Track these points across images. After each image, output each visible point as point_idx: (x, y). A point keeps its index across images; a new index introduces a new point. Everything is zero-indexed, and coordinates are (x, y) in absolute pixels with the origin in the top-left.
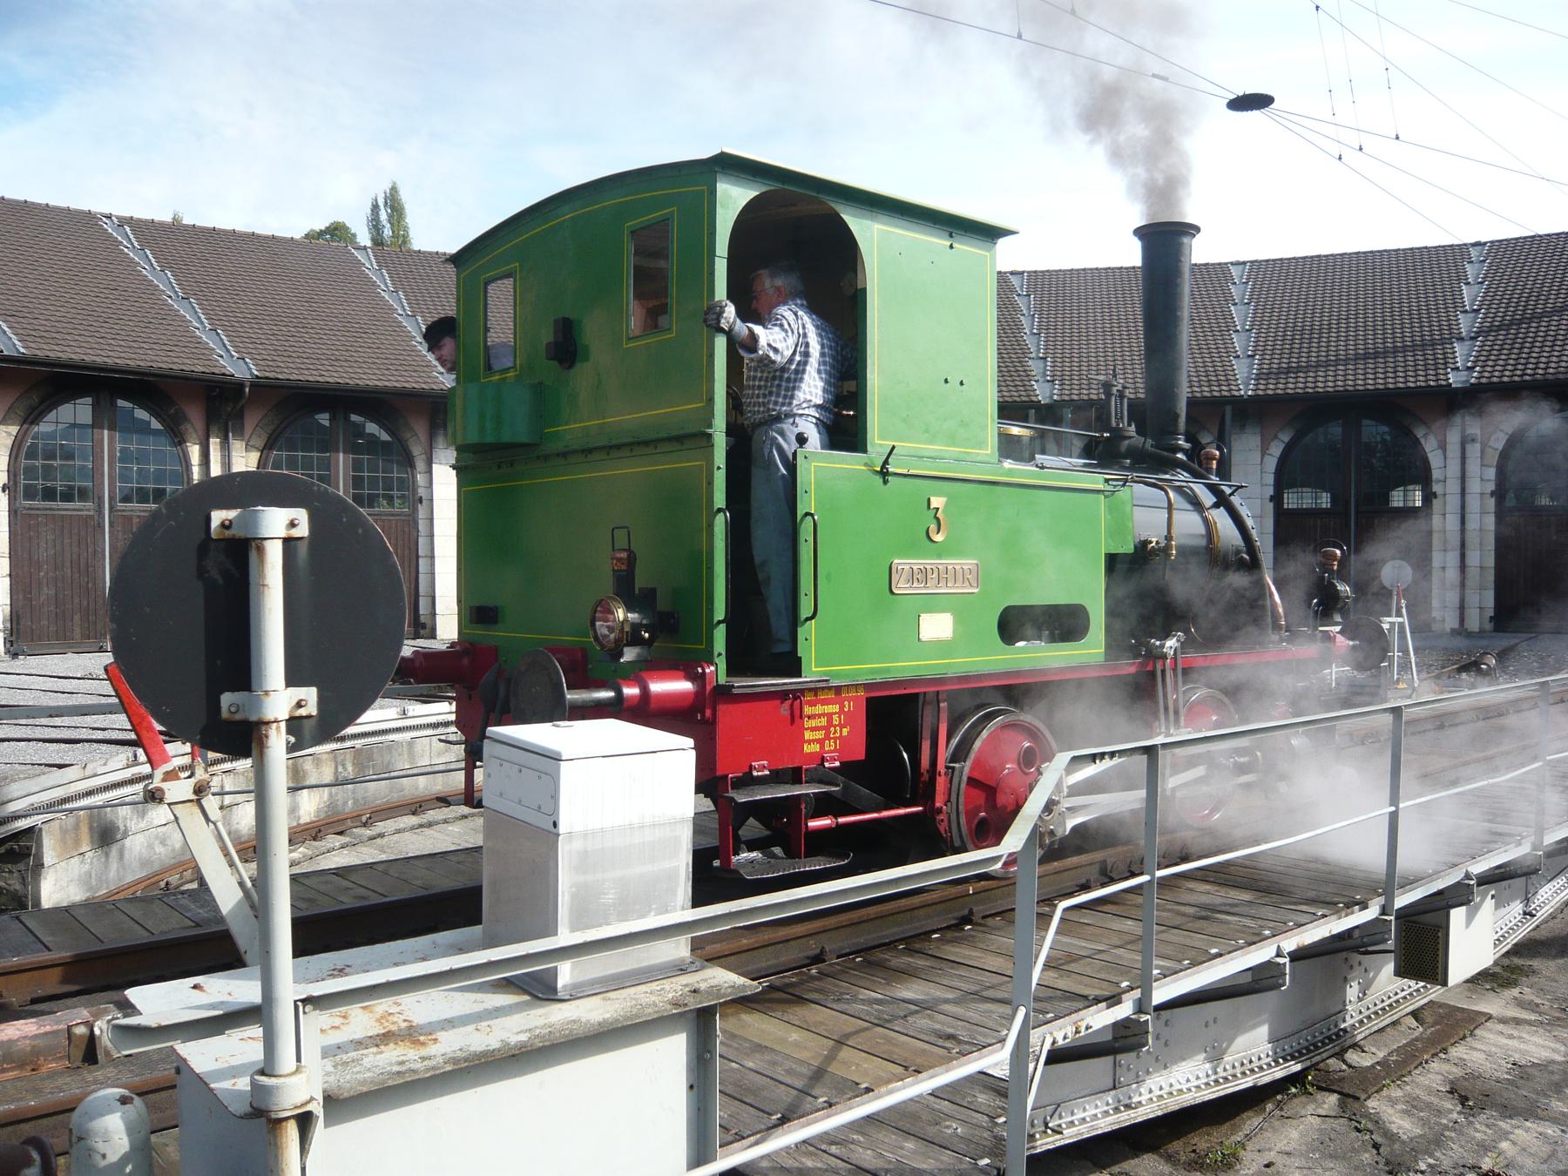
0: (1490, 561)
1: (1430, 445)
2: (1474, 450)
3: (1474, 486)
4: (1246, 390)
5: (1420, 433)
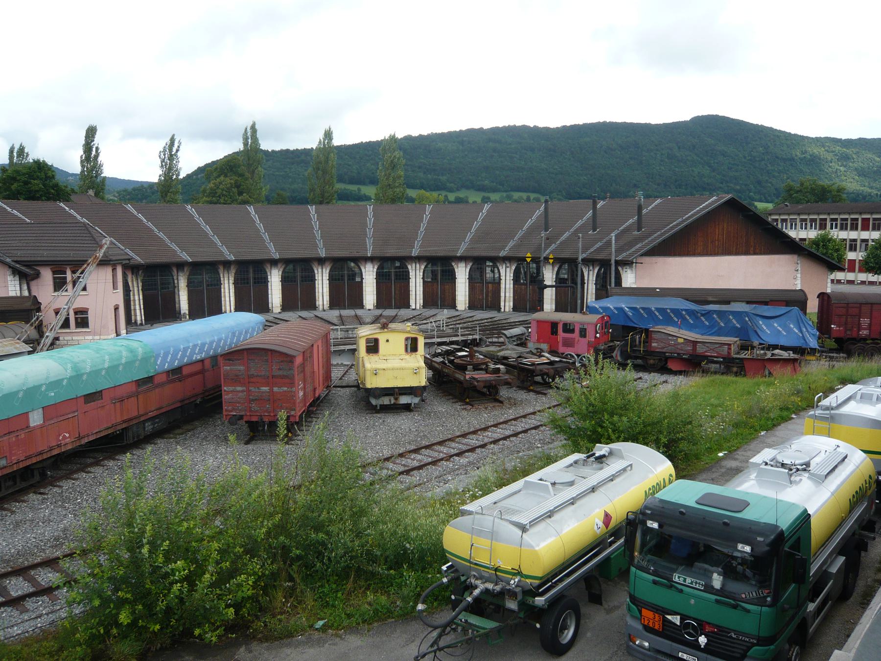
0: (512, 295)
1: (409, 267)
2: (591, 273)
3: (508, 278)
4: (369, 255)
5: (360, 265)
